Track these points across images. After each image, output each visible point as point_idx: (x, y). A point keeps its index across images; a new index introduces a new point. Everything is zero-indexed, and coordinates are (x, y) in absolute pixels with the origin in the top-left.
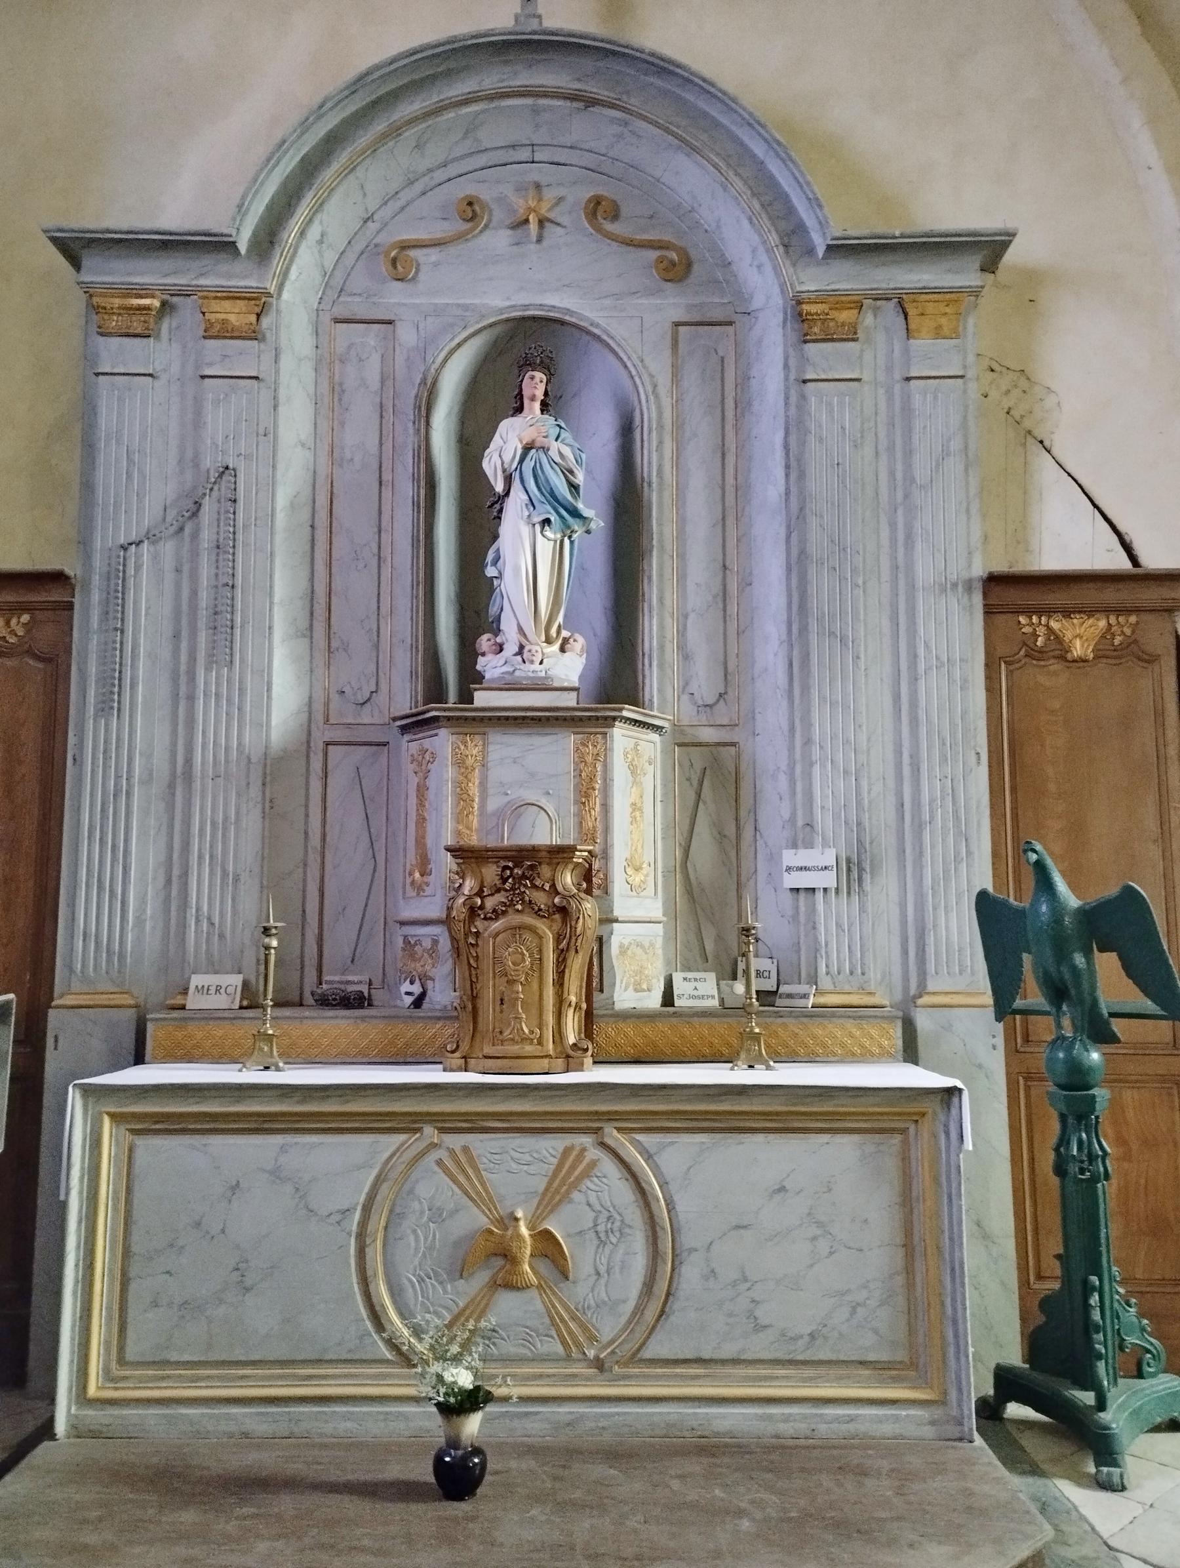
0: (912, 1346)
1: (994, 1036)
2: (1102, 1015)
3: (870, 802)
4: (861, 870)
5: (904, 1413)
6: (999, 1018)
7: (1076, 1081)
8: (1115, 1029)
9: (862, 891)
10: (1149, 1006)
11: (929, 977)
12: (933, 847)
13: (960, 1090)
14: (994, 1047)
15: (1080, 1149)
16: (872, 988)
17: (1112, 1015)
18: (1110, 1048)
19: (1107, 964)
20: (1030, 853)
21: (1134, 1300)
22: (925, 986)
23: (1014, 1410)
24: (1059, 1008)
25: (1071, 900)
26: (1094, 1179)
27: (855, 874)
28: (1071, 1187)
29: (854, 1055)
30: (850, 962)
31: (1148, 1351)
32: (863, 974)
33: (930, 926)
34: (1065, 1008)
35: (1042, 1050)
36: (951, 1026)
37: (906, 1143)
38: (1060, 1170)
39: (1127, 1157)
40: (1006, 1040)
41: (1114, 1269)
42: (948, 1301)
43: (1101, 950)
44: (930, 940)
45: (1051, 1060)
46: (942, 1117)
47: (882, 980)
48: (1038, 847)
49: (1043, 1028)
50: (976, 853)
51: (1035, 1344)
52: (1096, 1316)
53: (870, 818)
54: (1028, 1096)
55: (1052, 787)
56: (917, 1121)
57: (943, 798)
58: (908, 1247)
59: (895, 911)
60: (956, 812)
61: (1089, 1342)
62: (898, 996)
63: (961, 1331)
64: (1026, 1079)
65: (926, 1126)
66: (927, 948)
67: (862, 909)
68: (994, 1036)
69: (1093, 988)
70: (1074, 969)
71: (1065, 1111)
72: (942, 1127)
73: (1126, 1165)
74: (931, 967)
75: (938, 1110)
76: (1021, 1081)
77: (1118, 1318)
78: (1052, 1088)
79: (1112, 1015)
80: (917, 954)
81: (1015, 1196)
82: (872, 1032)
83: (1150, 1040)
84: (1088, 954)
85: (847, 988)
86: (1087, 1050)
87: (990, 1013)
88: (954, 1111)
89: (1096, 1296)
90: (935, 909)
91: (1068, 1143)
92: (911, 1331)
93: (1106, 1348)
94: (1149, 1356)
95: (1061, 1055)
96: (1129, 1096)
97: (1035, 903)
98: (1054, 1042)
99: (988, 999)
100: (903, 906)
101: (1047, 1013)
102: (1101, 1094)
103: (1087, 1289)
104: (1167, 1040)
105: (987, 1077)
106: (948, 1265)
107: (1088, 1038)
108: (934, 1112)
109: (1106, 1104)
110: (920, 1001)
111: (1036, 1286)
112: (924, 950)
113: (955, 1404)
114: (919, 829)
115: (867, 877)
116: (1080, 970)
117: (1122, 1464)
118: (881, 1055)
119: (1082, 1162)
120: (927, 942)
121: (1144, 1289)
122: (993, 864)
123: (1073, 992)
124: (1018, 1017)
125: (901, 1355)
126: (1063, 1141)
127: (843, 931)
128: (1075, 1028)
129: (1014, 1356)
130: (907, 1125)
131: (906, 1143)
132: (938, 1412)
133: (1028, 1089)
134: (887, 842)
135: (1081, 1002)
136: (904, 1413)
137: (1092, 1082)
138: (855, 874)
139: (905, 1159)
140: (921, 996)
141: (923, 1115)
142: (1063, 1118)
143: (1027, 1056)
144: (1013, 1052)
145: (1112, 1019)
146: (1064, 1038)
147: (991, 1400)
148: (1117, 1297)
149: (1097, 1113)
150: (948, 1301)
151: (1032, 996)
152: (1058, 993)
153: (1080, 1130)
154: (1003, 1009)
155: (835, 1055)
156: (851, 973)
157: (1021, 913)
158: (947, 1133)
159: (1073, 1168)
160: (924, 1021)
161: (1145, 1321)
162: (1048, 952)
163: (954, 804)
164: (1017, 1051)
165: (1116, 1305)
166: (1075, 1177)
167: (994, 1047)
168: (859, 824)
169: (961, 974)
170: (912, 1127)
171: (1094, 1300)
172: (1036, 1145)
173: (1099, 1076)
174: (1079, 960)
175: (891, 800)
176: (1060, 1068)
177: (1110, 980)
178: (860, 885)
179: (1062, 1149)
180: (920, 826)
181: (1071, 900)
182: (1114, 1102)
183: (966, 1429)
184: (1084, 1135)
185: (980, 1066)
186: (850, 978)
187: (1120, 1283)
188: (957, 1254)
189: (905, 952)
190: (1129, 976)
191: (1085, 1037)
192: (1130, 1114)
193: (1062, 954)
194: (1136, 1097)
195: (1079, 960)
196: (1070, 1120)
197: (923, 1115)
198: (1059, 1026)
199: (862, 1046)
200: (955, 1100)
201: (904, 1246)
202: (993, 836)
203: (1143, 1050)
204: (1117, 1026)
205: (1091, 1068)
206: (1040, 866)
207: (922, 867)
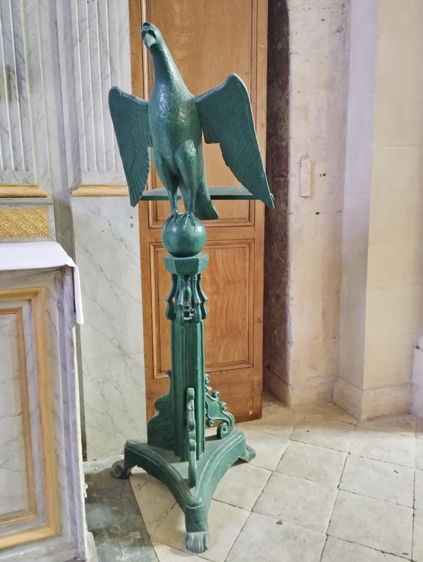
0: (31, 496)
1: (132, 218)
2: (205, 197)
3: (26, 16)
4: (20, 79)
5: (22, 553)
6: (133, 204)
7: (184, 249)
8: (214, 208)
9: (22, 99)
10: (240, 188)
11: (82, 173)
12: (83, 63)
13: (72, 269)
14: (132, 226)
15: (186, 298)
16: (36, 182)
17: (214, 197)
18: (211, 223)
19: (212, 152)
20: (148, 36)
21: (217, 393)
22: (80, 181)
23: (136, 470)
24: (174, 191)
25: (186, 94)
26: (194, 321)
27: (15, 82)
28: (179, 328)
29: (11, 236)
30: (15, 160)
31: (224, 421)
32: (27, 170)
33: (82, 130)
34: (179, 192)
35: (160, 226)
36: (99, 210)
37: (19, 322)
38: (172, 315)
39: (217, 292)
40: (141, 220)
41: (206, 375)
42: (63, 455)
43: (207, 142)
44: (83, 143)
45: (167, 234)
46: (55, 294)
47: (45, 174)
48: (157, 32)
49: (165, 209)
50: (119, 70)
51: (153, 429)
52: (191, 419)
53: (27, 32)
54: (156, 258)
55: (178, 22)
56: (30, 301)
57: (90, 20)
58: (25, 415)
59: (53, 117)
60: (101, 33)
61: (186, 437)
62: (59, 188)
63: (75, 479)
64: (155, 247)
65: (38, 302)
66: (81, 149)
67: (23, 114)
68: (132, 218)
69: (200, 177)
70: (185, 157)
71: (175, 272)
72: (56, 304)
73: (215, 297)
74: (84, 165)
75: (52, 288)
76: (152, 247)
77: (207, 407)
78: (169, 256)
79: (214, 197)
80: (73, 155)
81: (145, 329)
82: (27, 216)
83: (235, 216)
84: (198, 144)
85: (13, 182)
86: (194, 225)
87: (128, 199)
88: (67, 288)
89: (193, 401)
90: (86, 117)
91: (178, 294)
92: (30, 482)
93: (197, 441)
94: (225, 424)
95: (174, 229)
96: (220, 254)
97: (154, 97)
98: (169, 220)
99: (126, 190)
100: (60, 114)
101: (166, 198)
102: (202, 257)
103: (186, 399)
104: (244, 217)
105: (126, 247)
106: (63, 425)
107: (195, 214)
108: (48, 290)
109: (206, 265)
110: (75, 192)
111: (158, 377)
112: (78, 152)
113: (69, 533)
114: (71, 47)
115: (26, 85)
116: (191, 158)
117: (204, 527)
118: (38, 235)
119: (187, 308)
120: (80, 145)
121: (222, 369)
122: (133, 83)
123: (184, 176)
124: (150, 202)
125: (23, 505)
126: (174, 293)
127: (7, 132)
128: (189, 208)
129: (140, 436)
130: (19, 305)
131: (19, 322)
132: (52, 544)
133: (156, 253)
134: (43, 55)
135: (191, 187)
136: (22, 553)
137: (197, 250)
138: (15, 82)
139: (20, 336)
140: (76, 188)
141: (36, 294)
142: (175, 277)
143: (156, 231)
144: (146, 228)
145: (213, 201)
146: (177, 216)
147: (122, 466)
148: (207, 394)
149: (198, 273)
150: (63, 455)
151: (155, 185)
152: (174, 180)
153: (187, 285)
154: (136, 196)
155: (11, 236)
156: (16, 169)
157: (145, 108)
158: (61, 310)
159: (180, 314)
160: (78, 207)
161: (224, 403)
162: (165, 139)
163: (100, 26)
164: (149, 228)
165: (206, 399)
166: (181, 318)
167: (132, 226)
168: (16, 36)
169: (108, 171)
170: (26, 308)
171: (191, 405)
172: (160, 288)
173: (201, 244)
174: (191, 149)
175: (46, 16)
176: (173, 240)
177: (214, 170)
178: (20, 93)
179: (174, 300)
180: (72, 43)
181: (186, 94)
182: (212, 262)
183: (80, 552)
184: (189, 289)
185: (121, 240)
186: (16, 173)
187: (209, 385)
188: (71, 416)
189: (63, 152)
190: (227, 164)
191: (192, 214)
192: (220, 266)
193: (175, 136)
194: (224, 254)
195: (191, 149)
196: (179, 280)
197: (36, 294)
198: (174, 206)
199: (36, 228)
200: (68, 279)
201: (22, 413)
202: (132, 59)
203: (231, 224)
204: (216, 205)
205: (196, 240)
206: (155, 50)
207: (74, 80)
